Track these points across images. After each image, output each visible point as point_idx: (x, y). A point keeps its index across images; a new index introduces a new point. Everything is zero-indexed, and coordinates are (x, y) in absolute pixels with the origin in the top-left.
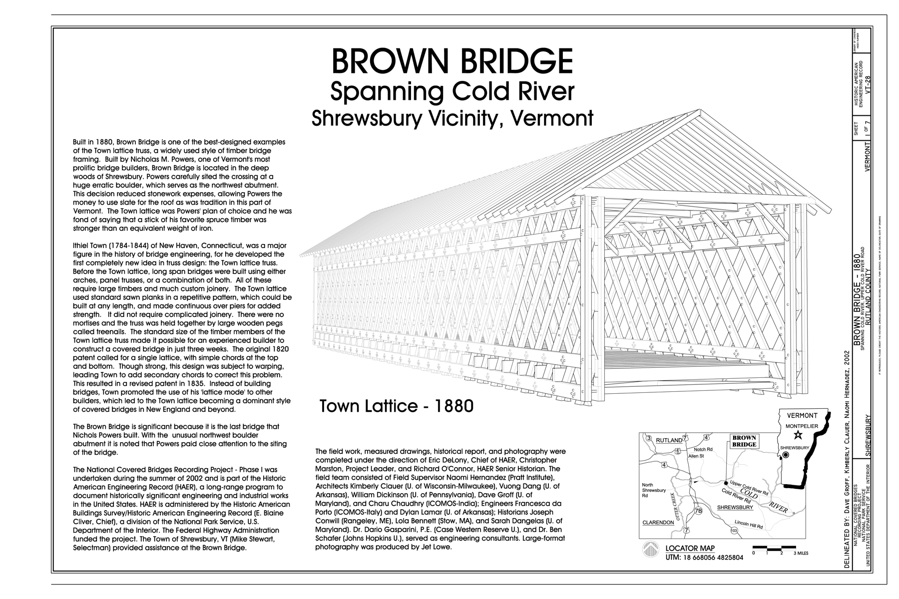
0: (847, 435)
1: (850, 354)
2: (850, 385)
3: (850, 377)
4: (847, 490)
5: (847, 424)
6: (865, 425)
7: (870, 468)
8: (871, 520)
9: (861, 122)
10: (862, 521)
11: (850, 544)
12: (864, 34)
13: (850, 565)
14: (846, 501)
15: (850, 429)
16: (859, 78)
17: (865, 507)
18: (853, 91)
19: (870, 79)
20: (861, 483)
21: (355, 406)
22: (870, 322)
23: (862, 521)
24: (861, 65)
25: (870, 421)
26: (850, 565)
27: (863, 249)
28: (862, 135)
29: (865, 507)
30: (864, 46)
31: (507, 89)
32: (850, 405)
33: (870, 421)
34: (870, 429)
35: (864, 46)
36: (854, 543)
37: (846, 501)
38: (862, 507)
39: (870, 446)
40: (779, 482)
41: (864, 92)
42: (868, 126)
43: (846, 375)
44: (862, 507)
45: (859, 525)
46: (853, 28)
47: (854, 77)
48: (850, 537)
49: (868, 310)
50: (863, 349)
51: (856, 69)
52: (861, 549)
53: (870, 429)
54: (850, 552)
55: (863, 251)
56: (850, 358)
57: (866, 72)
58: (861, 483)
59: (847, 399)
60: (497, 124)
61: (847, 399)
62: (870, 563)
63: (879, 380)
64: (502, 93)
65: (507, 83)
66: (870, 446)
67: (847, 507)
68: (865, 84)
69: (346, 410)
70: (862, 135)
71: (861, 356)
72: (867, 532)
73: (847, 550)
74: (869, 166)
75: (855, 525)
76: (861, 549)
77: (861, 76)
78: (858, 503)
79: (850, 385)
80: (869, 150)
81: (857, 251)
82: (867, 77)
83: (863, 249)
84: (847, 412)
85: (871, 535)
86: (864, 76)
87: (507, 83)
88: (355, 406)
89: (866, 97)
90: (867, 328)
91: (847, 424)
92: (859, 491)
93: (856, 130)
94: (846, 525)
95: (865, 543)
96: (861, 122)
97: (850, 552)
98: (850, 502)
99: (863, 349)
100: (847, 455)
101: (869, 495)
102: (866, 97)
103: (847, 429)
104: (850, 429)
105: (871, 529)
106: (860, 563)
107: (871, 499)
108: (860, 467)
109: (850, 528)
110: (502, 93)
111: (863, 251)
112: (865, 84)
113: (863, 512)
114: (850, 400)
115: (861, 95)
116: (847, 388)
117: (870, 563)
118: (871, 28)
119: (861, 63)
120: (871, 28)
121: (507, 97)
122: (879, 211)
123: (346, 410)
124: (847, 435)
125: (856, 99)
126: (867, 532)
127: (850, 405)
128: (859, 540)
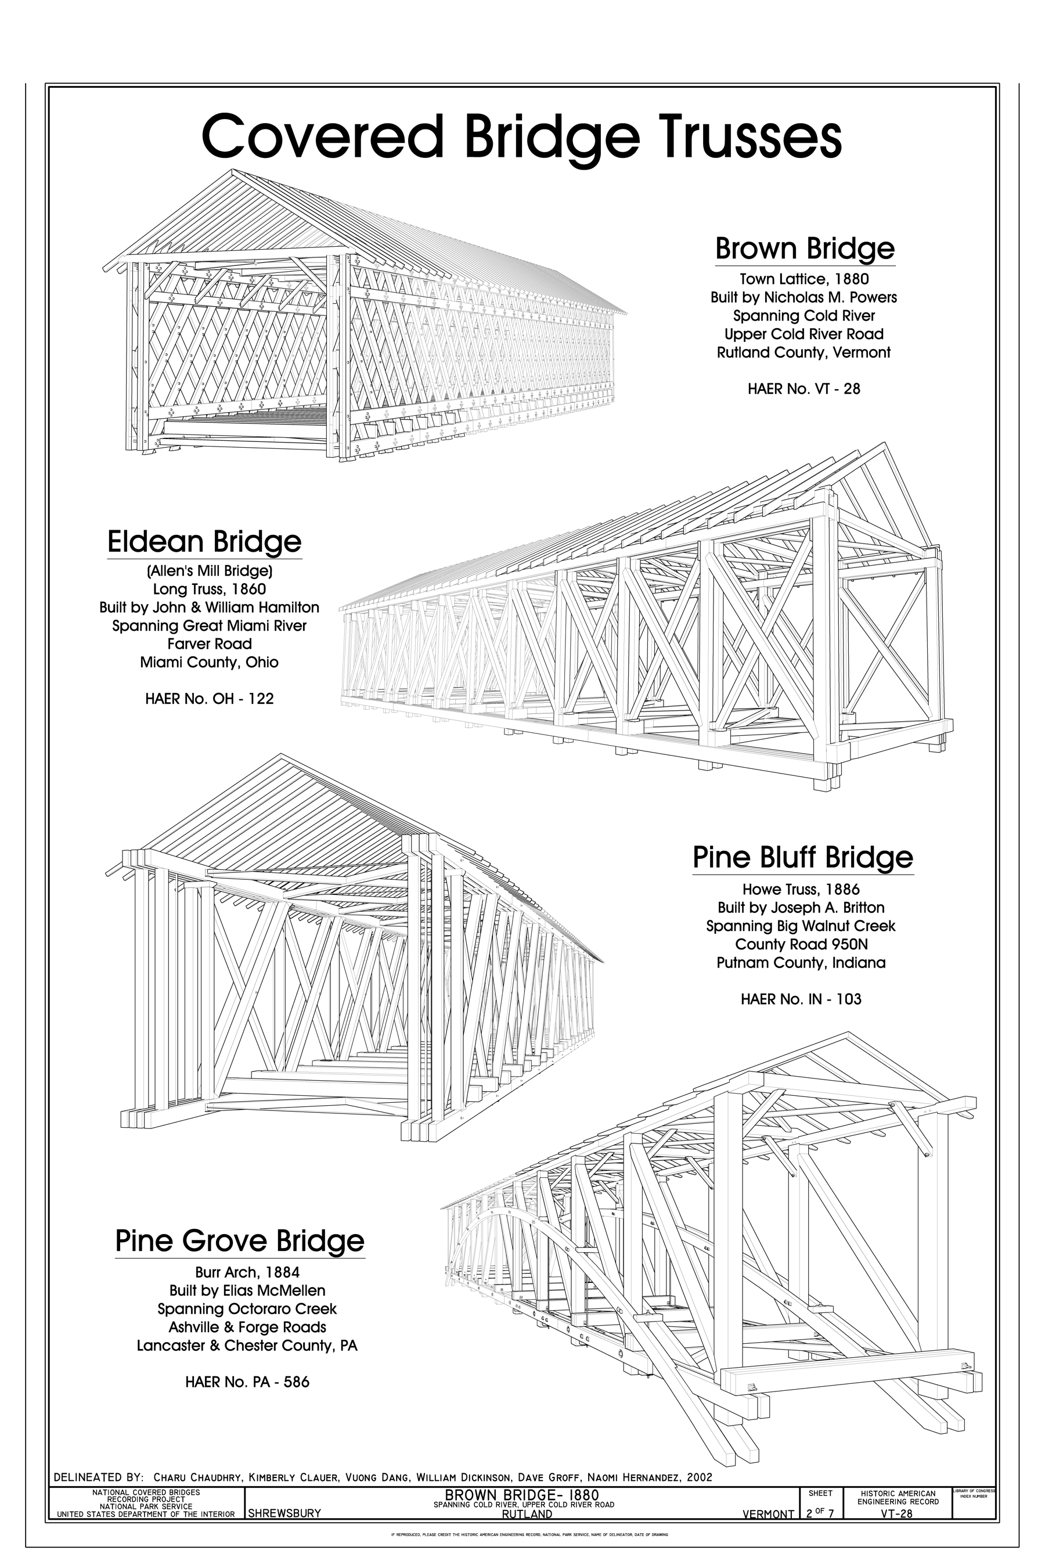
0: (316, 1478)
1: (706, 1483)
2: (645, 1483)
3: (667, 1483)
4: (559, 1477)
5: (335, 1477)
6: (303, 1507)
7: (227, 1518)
8: (137, 1519)
9: (831, 1502)
10: (137, 1505)
11: (96, 1483)
12: (984, 1507)
13: (60, 1483)
14: (540, 1476)
15: (326, 1483)
16: (908, 1499)
17: (160, 1509)
18: (885, 1489)
19: (907, 1518)
20: (204, 1502)
21: (771, 279)
22: (508, 1518)
23: (137, 1505)
24: (931, 1501)
25: (309, 1517)
26: (60, 1483)
27: (610, 1505)
28: (810, 1503)
29: (160, 1509)
30: (965, 1507)
31: (438, 131)
32: (611, 1483)
33: (309, 1517)
34: (294, 1517)
35: (965, 1507)
36: (97, 1491)
37: (540, 1476)
38: (160, 1504)
39: (268, 1516)
40: (656, 1372)
41: (885, 1507)
42: (826, 1514)
43: (670, 1476)
44: (160, 1504)
45: (129, 1499)
46: (995, 1488)
47: (909, 1490)
48: (107, 1483)
49: (529, 1515)
50: (437, 1505)
51: (926, 1493)
52: (88, 1502)
53: (294, 1517)
54: (82, 1483)
55: (607, 1505)
56: (700, 1483)
57: (918, 1511)
58: (204, 1502)
59: (620, 1477)
60: (823, 356)
61: (620, 1477)
62: (63, 1518)
63: (382, 1533)
64: (833, 317)
65: (439, 117)
66: (268, 1516)
67: (529, 1478)
68: (898, 1508)
69: (774, 255)
70: (810, 1503)
71: (424, 1502)
72: (117, 1511)
73: (86, 1477)
74: (750, 1517)
75: (130, 1491)
76: (88, 1502)
77: (912, 1502)
78: (168, 1496)
79: (645, 1483)
80: (781, 1517)
81: (604, 1495)
82: (910, 1512)
83: (610, 1505)
84: (207, 1478)
85: (111, 1519)
86: (913, 1507)
87: (439, 117)
88: (771, 279)
89: (875, 1511)
90: (498, 1513)
91: (335, 1477)
92: (188, 1499)
93: (819, 1493)
94: (130, 1477)
95: (98, 1509)
96: (831, 1502)
97: (82, 1483)
98: (537, 1483)
99: (437, 1505)
100: (281, 1477)
101: (181, 1515)
102: (875, 1511)
103: (327, 1477)
104: (326, 1483)
105: (123, 1519)
106: (63, 1501)
107: (174, 1519)
108: (229, 1501)
109: (124, 1482)
110: (833, 317)
111: (607, 1505)
112: (898, 1508)
113: (152, 1506)
114: (620, 1482)
115: (880, 1502)
116: (641, 1477)
117: (63, 1518)
118: (996, 1519)
119: (934, 1502)
120: (996, 1519)
121: (438, 151)
122: (677, 1533)
123: (774, 255)
124: (316, 1478)
125: (872, 1493)
126: (117, 1511)
127: (611, 1483)
128: (103, 1499)
